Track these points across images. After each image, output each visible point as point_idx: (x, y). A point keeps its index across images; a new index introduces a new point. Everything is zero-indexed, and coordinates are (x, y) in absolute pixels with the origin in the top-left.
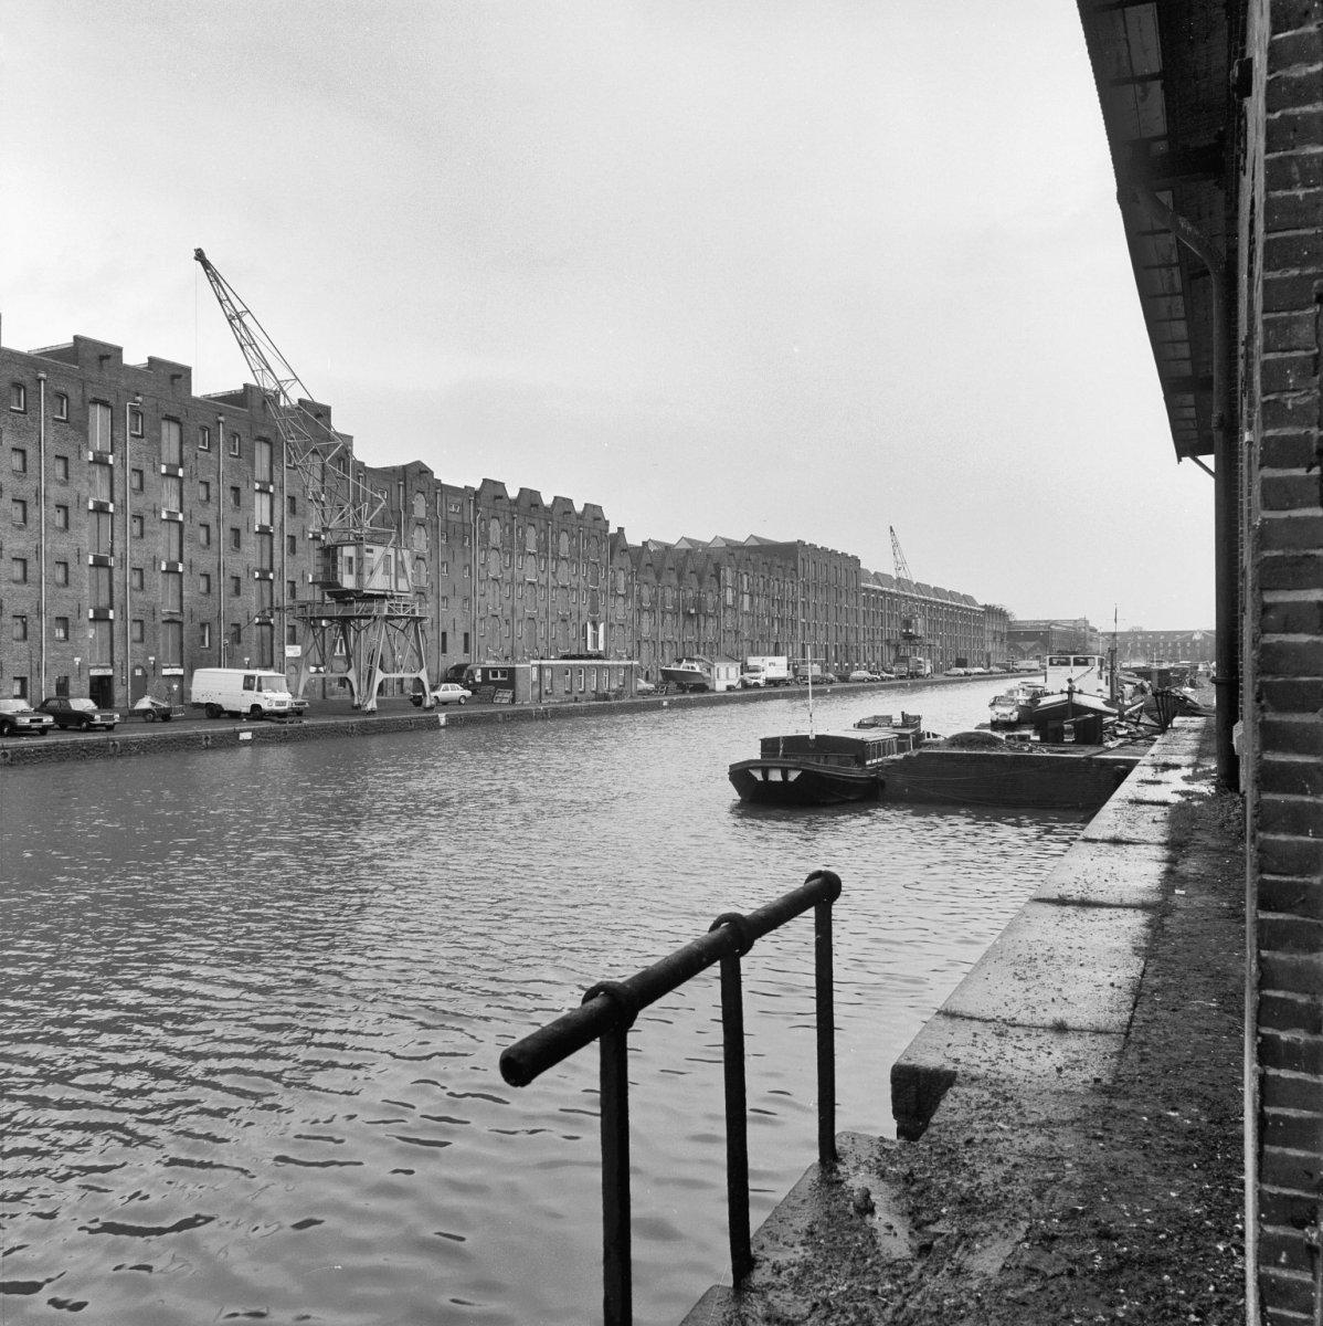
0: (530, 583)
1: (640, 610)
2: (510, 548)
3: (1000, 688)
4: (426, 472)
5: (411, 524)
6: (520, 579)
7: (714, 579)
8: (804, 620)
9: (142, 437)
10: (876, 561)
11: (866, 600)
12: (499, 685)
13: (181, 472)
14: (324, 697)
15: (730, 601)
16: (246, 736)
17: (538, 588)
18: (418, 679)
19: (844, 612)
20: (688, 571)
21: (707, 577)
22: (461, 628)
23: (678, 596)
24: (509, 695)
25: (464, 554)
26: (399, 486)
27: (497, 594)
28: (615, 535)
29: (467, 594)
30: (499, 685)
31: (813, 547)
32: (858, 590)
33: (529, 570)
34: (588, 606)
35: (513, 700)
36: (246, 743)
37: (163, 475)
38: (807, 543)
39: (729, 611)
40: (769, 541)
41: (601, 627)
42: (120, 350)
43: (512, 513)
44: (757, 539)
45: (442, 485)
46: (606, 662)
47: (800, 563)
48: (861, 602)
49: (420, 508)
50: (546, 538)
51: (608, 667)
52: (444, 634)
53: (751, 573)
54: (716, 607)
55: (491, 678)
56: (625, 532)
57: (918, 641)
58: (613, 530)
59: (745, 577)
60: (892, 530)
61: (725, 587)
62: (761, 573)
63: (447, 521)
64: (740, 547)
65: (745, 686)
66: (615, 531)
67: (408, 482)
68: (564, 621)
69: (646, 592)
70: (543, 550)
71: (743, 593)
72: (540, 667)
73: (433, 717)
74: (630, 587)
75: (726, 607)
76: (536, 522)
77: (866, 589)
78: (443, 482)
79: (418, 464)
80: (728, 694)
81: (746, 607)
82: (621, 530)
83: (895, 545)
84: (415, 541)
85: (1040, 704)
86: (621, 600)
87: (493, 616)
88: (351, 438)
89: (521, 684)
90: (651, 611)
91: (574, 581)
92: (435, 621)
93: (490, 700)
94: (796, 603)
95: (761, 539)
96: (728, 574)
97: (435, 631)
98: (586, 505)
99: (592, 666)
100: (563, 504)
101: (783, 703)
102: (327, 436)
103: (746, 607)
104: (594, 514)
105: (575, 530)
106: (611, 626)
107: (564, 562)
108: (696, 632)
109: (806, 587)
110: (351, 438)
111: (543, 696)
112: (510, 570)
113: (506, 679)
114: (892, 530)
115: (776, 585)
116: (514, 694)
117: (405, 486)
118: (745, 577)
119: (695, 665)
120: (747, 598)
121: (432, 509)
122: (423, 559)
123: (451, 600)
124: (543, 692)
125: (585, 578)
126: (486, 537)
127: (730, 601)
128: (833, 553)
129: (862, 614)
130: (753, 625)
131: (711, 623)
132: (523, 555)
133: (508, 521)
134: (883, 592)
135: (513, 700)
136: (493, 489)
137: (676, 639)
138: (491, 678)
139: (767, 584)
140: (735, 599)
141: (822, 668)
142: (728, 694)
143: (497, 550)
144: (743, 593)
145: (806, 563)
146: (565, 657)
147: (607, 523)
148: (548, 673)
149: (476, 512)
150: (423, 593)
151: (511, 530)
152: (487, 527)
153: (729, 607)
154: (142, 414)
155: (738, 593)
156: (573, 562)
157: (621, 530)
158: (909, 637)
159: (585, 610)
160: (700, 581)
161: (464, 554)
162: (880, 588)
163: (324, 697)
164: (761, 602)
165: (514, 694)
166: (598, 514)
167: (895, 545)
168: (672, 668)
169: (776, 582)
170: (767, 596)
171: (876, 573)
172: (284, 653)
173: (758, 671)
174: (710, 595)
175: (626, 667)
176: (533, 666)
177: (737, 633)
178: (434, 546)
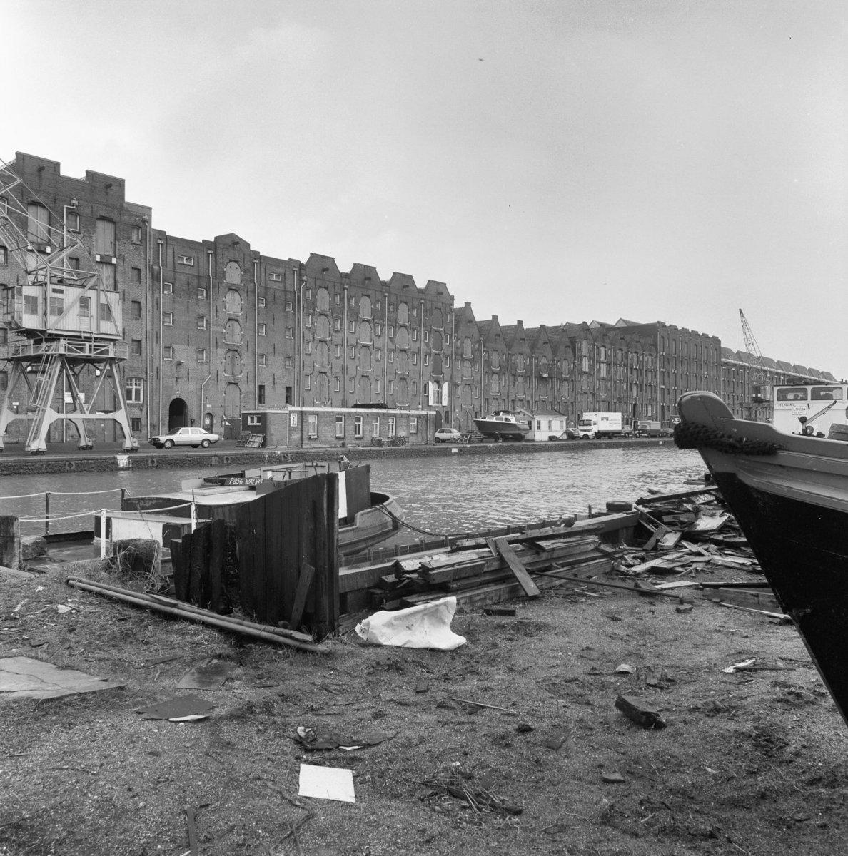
0: (364, 346)
1: (489, 373)
2: (336, 314)
3: (35, 537)
4: (238, 243)
5: (221, 289)
6: (352, 341)
7: (570, 350)
8: (663, 387)
9: (79, 233)
10: (732, 342)
11: (727, 373)
12: (254, 429)
13: (114, 261)
14: (115, 440)
15: (586, 367)
16: (455, 450)
17: (373, 351)
18: (115, 421)
19: (731, 384)
20: (541, 342)
21: (562, 348)
22: (283, 382)
23: (531, 363)
24: (259, 439)
25: (286, 317)
26: (208, 254)
27: (326, 355)
28: (460, 309)
29: (290, 353)
30: (254, 429)
31: (673, 328)
32: (718, 365)
33: (365, 335)
34: (430, 369)
35: (264, 445)
36: (455, 454)
37: (97, 262)
38: (690, 331)
39: (585, 377)
40: (634, 323)
41: (445, 387)
42: (120, 183)
43: (343, 284)
44: (625, 321)
45: (261, 256)
46: (391, 411)
47: (659, 340)
48: (721, 373)
49: (233, 274)
50: (383, 308)
51: (395, 416)
52: (262, 388)
53: (609, 346)
54: (571, 373)
55: (249, 423)
56: (472, 306)
57: (766, 404)
58: (458, 304)
59: (603, 350)
60: (741, 312)
61: (582, 357)
62: (634, 350)
63: (266, 288)
64: (612, 328)
65: (571, 436)
66: (463, 306)
67: (219, 251)
68: (403, 379)
69: (495, 358)
70: (378, 318)
71: (600, 362)
72: (302, 414)
73: (111, 459)
74: (477, 353)
75: (581, 373)
76: (370, 293)
77: (726, 364)
78: (167, 234)
79: (231, 236)
80: (550, 443)
81: (603, 373)
82: (468, 304)
83: (745, 325)
84: (227, 305)
85: (574, 526)
86: (467, 364)
87: (320, 373)
88: (150, 209)
89: (273, 429)
90: (501, 374)
91: (415, 347)
92: (251, 375)
93: (243, 443)
94: (656, 372)
95: (629, 322)
96: (584, 346)
97: (251, 385)
98: (429, 281)
99: (373, 414)
100: (403, 281)
101: (619, 451)
102: (120, 204)
103: (603, 373)
104: (437, 291)
105: (416, 303)
106: (456, 386)
107: (403, 329)
108: (549, 394)
109: (666, 359)
110: (150, 209)
111: (305, 441)
112: (382, 339)
113: (259, 424)
114: (741, 312)
115: (650, 360)
116: (265, 438)
117: (215, 255)
118: (603, 350)
119: (509, 417)
120: (604, 367)
121: (248, 277)
122: (237, 320)
123: (271, 359)
124: (305, 437)
125: (427, 344)
126: (312, 304)
127: (586, 367)
128: (695, 334)
129: (721, 383)
130: (610, 390)
131: (566, 386)
132: (356, 321)
133: (338, 291)
134: (742, 367)
135: (264, 445)
136: (321, 266)
137: (529, 398)
138: (249, 423)
139: (625, 356)
140: (592, 367)
141: (662, 424)
142: (550, 443)
143: (326, 315)
144: (600, 362)
145: (666, 342)
146: (356, 406)
147: (452, 298)
148: (312, 420)
149: (300, 281)
150: (236, 351)
151: (342, 300)
152: (313, 295)
153: (585, 373)
154: (79, 215)
155: (595, 361)
156: (413, 330)
157: (468, 304)
158: (759, 401)
159: (427, 371)
160: (555, 352)
161: (286, 317)
162: (798, 375)
163: (115, 440)
164: (620, 372)
165: (265, 438)
166: (441, 290)
167: (745, 325)
168: (487, 420)
169: (635, 355)
170: (625, 366)
171: (778, 361)
172: (63, 399)
173: (590, 425)
174: (565, 364)
175: (419, 417)
176: (290, 412)
177: (593, 395)
178: (249, 310)
